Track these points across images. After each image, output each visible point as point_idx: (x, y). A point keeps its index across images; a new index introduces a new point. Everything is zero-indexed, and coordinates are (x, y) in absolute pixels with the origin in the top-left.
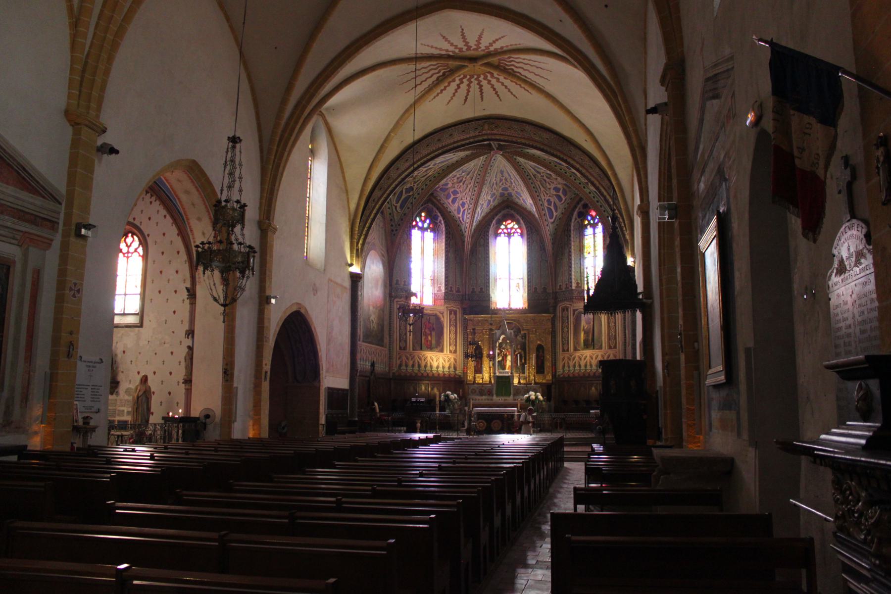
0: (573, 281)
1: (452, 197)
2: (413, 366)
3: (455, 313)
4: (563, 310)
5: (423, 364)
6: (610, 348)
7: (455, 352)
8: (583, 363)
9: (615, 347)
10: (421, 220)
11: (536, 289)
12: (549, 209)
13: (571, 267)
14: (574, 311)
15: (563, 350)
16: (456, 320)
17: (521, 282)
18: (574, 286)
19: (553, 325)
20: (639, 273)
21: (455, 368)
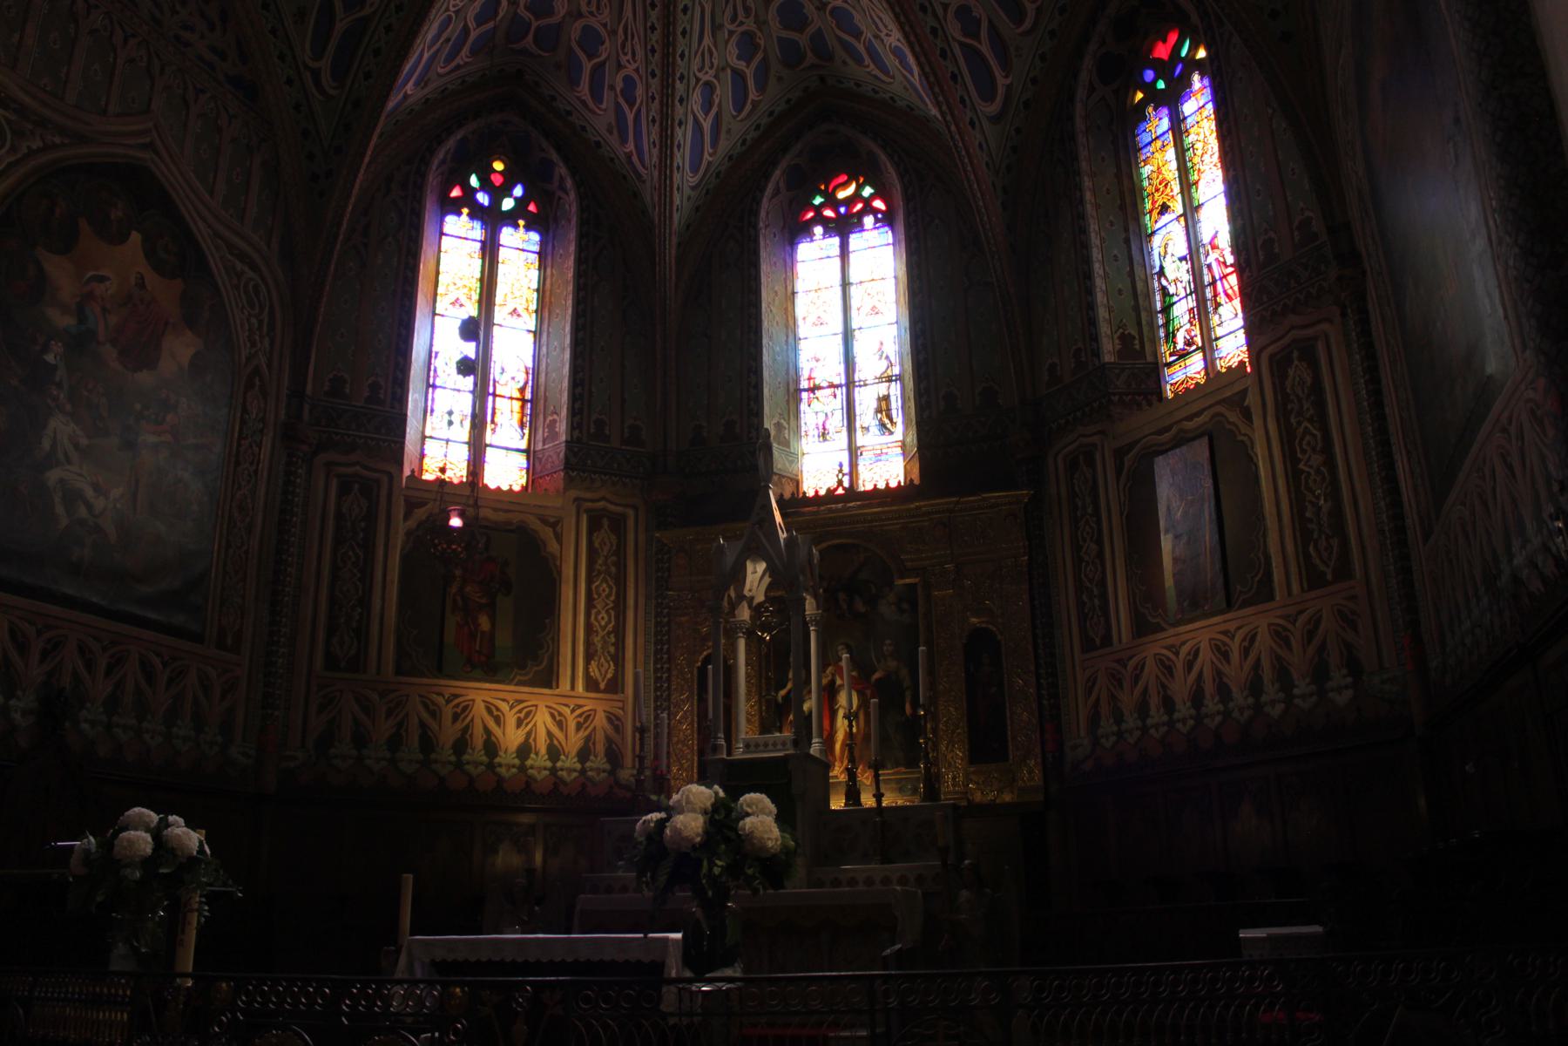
0: (1104, 329)
1: (588, 66)
2: (395, 742)
3: (618, 525)
5: (448, 733)
6: (1314, 580)
7: (615, 686)
8: (1180, 688)
9: (1343, 571)
10: (486, 185)
12: (973, 55)
13: (1089, 276)
14: (1119, 454)
15: (1088, 645)
17: (895, 390)
18: (1109, 349)
21: (613, 756)
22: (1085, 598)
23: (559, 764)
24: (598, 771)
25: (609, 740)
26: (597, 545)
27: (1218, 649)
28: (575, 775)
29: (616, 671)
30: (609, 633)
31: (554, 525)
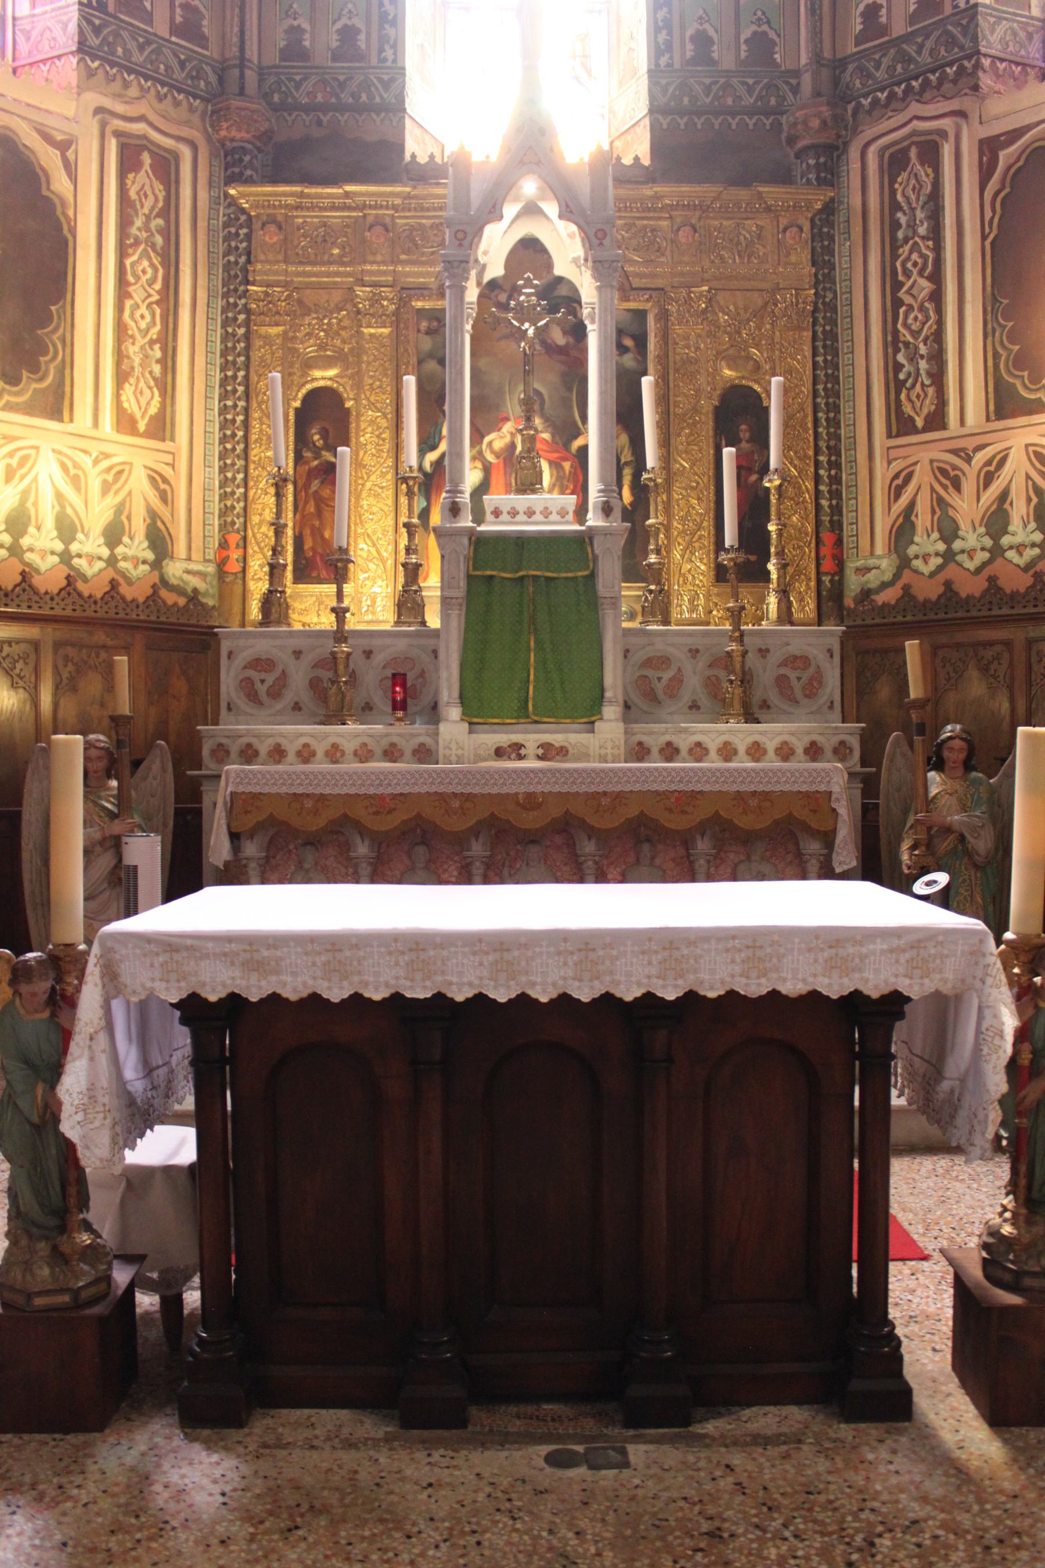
3: (166, 168)
4: (895, 162)
7: (161, 427)
11: (702, 41)
14: (990, 147)
15: (901, 425)
16: (169, 210)
19: (823, 261)
20: (972, 254)
21: (159, 541)
22: (901, 358)
23: (74, 548)
24: (137, 561)
25: (153, 515)
26: (133, 194)
27: (943, 472)
28: (101, 565)
29: (163, 404)
30: (152, 342)
31: (63, 146)
